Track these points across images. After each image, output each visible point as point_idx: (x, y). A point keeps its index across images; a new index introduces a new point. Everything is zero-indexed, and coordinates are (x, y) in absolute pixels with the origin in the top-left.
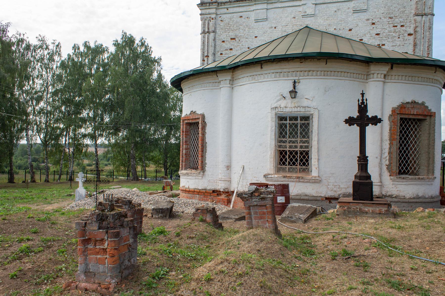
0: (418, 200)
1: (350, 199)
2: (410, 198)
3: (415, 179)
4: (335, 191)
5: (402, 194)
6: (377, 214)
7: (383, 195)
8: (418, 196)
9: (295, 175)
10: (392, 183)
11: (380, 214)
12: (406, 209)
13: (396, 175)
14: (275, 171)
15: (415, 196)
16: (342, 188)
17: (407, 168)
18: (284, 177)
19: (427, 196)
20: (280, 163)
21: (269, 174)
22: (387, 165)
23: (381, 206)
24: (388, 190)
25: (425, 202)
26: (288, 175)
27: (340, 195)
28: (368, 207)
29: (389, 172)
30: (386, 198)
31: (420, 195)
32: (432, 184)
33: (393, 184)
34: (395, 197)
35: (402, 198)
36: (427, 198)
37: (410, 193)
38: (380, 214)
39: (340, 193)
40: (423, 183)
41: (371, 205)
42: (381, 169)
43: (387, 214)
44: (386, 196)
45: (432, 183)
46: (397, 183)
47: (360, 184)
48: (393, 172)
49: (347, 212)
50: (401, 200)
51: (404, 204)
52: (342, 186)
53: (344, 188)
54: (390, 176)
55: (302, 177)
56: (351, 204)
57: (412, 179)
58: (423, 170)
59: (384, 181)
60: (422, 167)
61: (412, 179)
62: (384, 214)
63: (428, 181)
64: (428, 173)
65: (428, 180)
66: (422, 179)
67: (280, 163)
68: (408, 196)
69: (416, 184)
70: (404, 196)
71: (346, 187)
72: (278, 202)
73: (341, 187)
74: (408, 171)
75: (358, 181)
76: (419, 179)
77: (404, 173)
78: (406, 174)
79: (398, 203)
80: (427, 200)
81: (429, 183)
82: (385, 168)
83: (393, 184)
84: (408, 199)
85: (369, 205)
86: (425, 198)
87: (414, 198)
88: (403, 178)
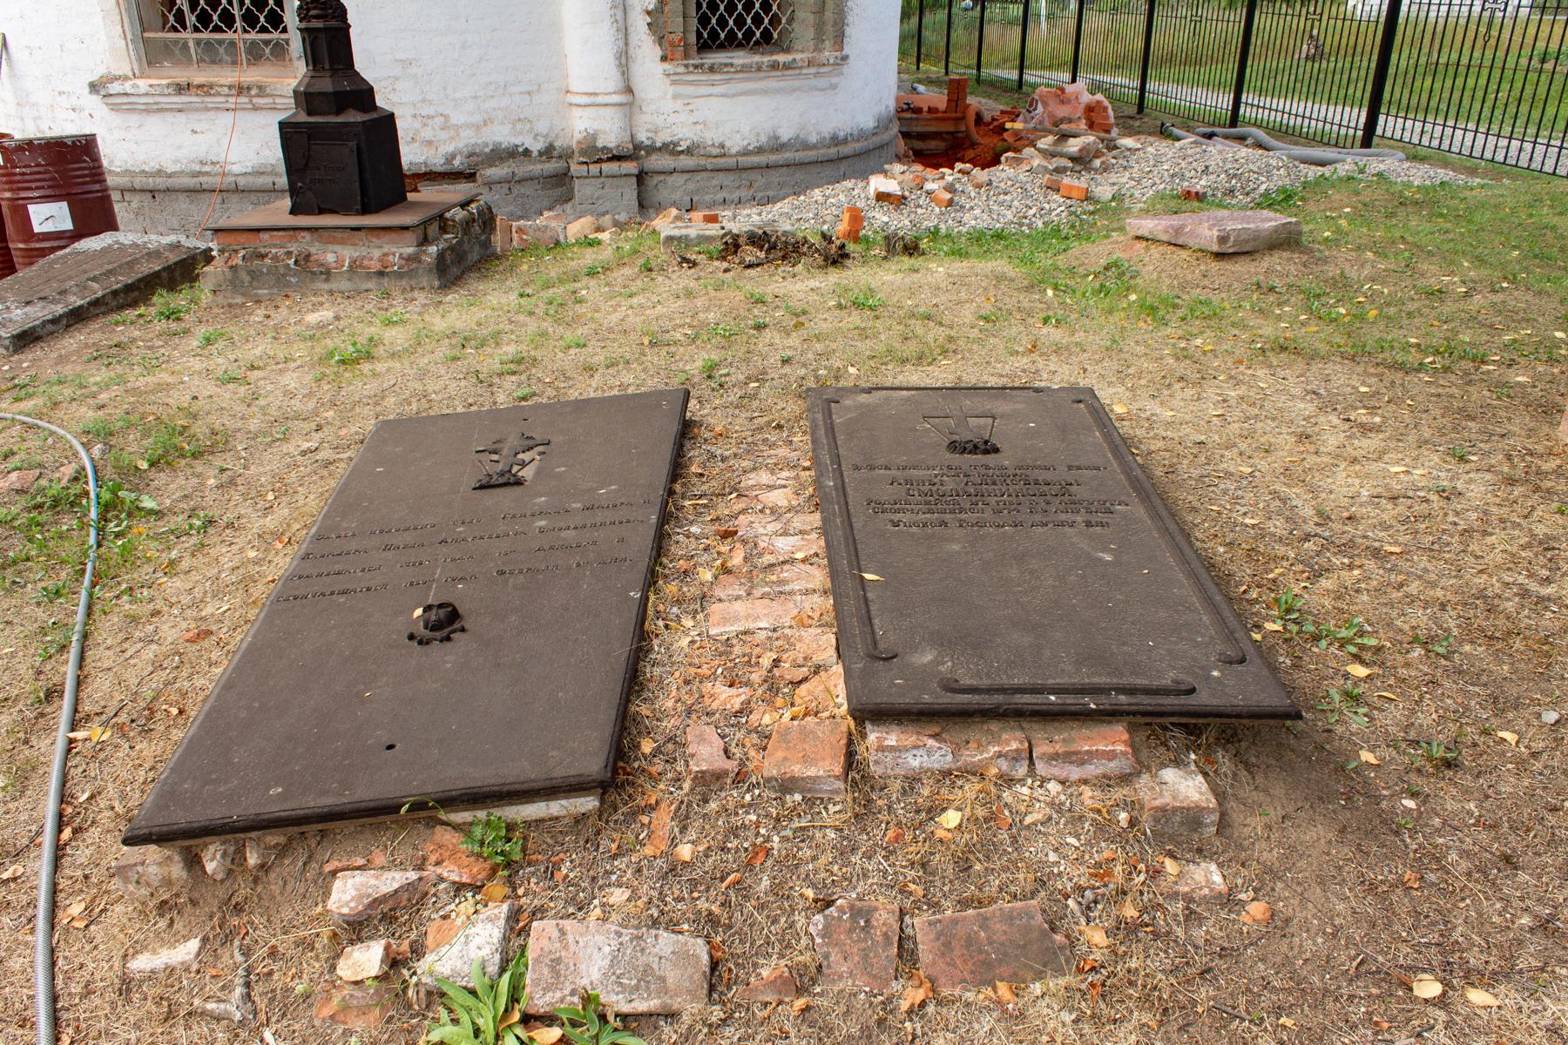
0: (773, 158)
1: (279, 211)
2: (746, 153)
3: (759, 69)
4: (430, 143)
5: (711, 136)
6: (369, 276)
7: (637, 147)
8: (777, 138)
9: (226, 76)
10: (671, 90)
11: (381, 274)
12: (728, 196)
13: (686, 56)
14: (139, 60)
15: (764, 139)
16: (457, 128)
17: (740, 22)
18: (180, 89)
19: (813, 139)
20: (165, 20)
21: (117, 78)
22: (649, 13)
23: (387, 237)
24: (660, 121)
25: (802, 164)
26: (198, 80)
27: (453, 156)
28: (336, 247)
29: (660, 40)
30: (654, 157)
31: (786, 134)
32: (834, 87)
33: (675, 97)
34: (689, 151)
35: (715, 151)
36: (814, 147)
37: (746, 130)
38: (381, 274)
39: (451, 149)
40: (797, 83)
41: (347, 234)
42: (625, 32)
43: (411, 274)
44: (651, 149)
45: (834, 80)
46: (690, 90)
47: (312, 132)
48: (672, 44)
49: (247, 278)
50: (710, 163)
51: (721, 178)
52: (457, 118)
53: (468, 126)
54: (664, 59)
55: (260, 88)
56: (265, 236)
57: (744, 69)
58: (803, 29)
59: (639, 84)
60: (800, 15)
61: (744, 69)
62: (399, 275)
63: (816, 75)
64: (819, 38)
65: (813, 70)
66: (787, 67)
67: (165, 20)
68: (735, 144)
69: (766, 92)
70: (723, 146)
71: (477, 118)
72: (37, 229)
73: (454, 121)
74: (749, 34)
75: (303, 118)
76: (774, 66)
77: (731, 43)
78: (740, 46)
79: (699, 177)
80: (811, 155)
81: (822, 82)
82: (640, 23)
83: (675, 97)
84: (740, 154)
85: (338, 235)
86: (806, 146)
87: (760, 150)
88: (712, 69)
